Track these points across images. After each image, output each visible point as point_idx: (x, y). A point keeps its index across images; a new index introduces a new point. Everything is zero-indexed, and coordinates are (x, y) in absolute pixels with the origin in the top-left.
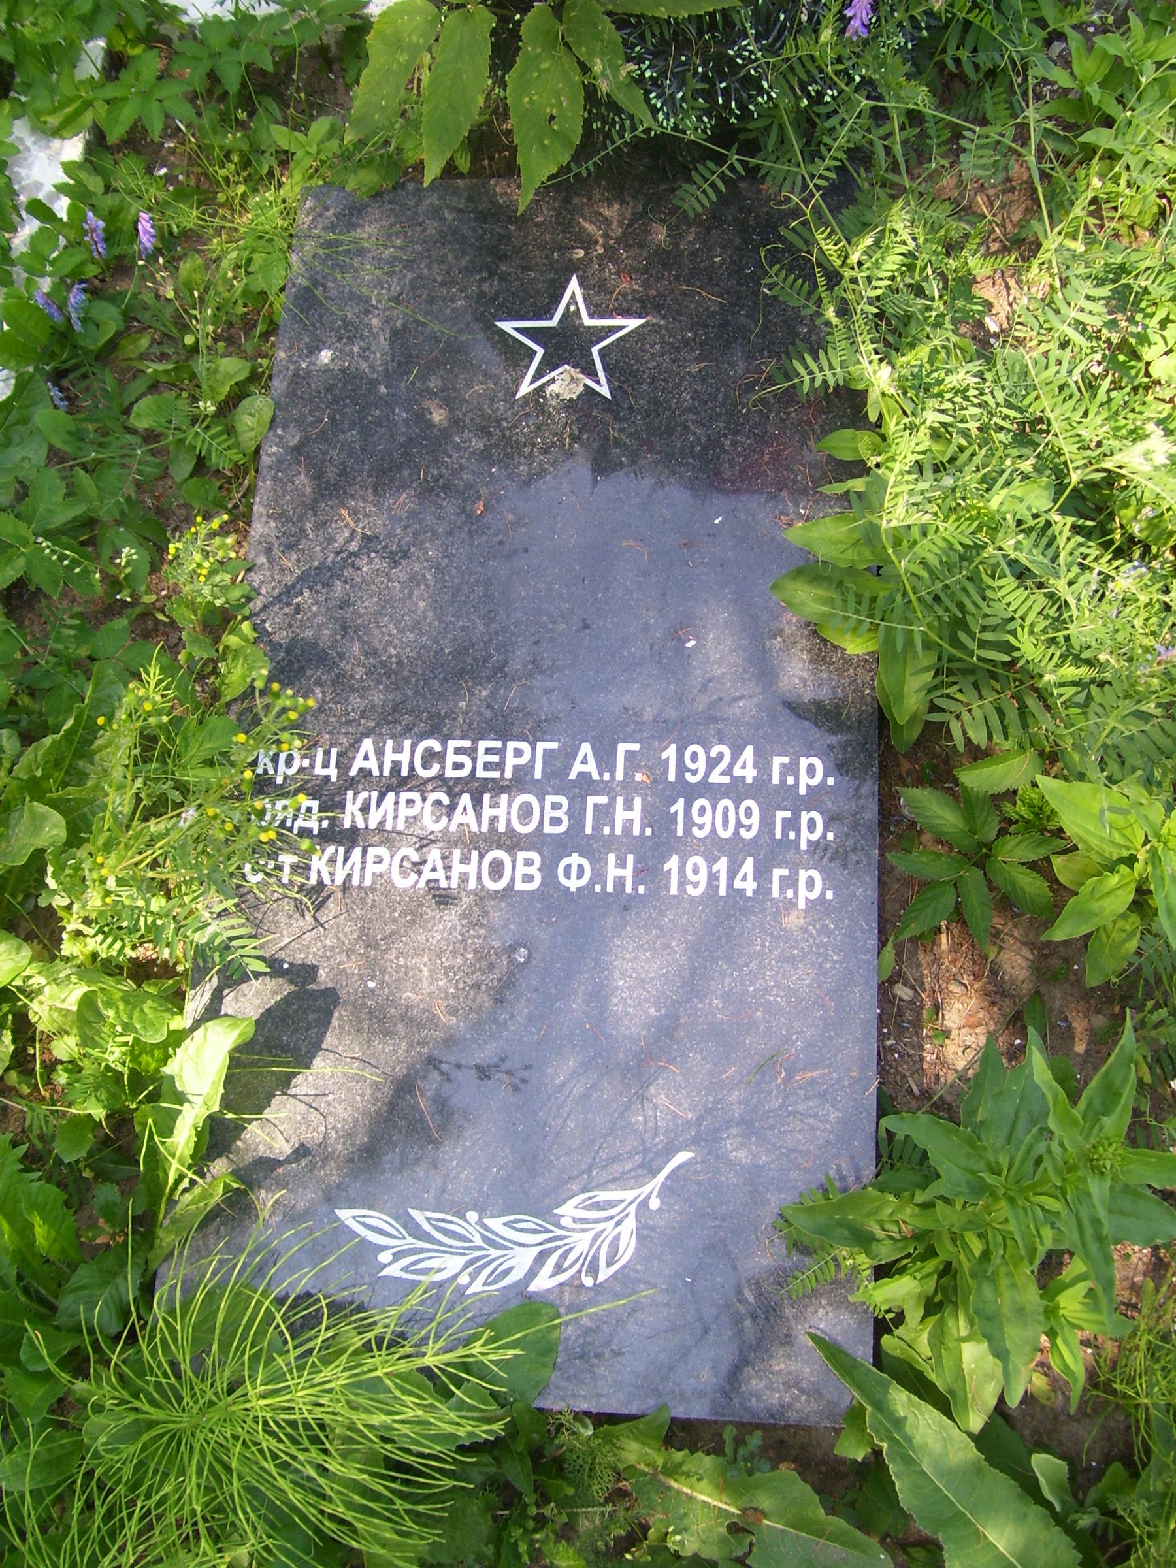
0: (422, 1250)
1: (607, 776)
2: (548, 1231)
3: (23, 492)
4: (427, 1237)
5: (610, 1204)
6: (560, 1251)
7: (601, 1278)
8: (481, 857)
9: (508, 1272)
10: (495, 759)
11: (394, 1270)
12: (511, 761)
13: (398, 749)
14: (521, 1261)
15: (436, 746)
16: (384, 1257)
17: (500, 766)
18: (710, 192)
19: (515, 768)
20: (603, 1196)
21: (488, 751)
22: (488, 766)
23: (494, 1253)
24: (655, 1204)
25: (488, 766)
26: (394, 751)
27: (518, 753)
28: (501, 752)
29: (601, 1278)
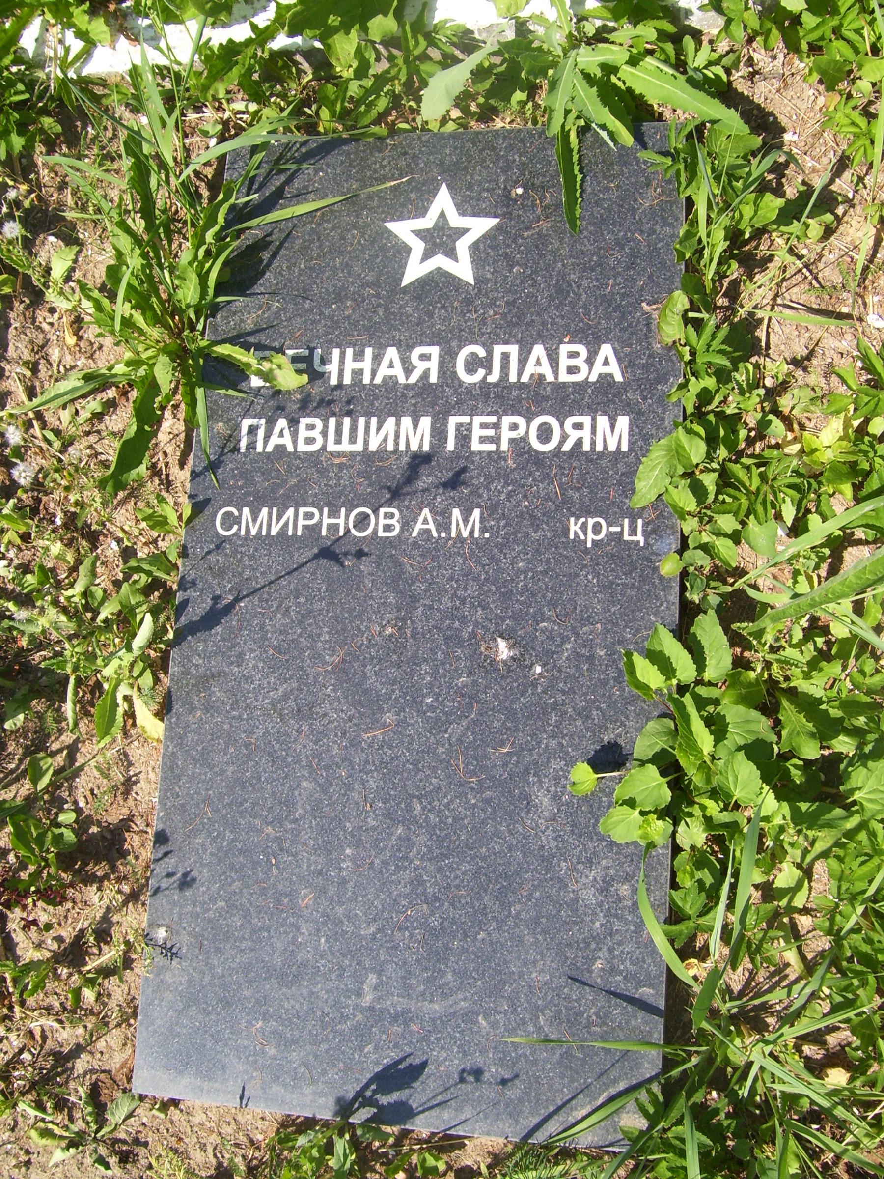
3: (821, 788)
8: (375, 531)
10: (491, 432)
12: (506, 435)
13: (358, 374)
15: (481, 352)
17: (496, 440)
19: (511, 441)
21: (484, 426)
22: (483, 440)
25: (483, 440)
26: (355, 360)
27: (514, 427)
28: (497, 426)
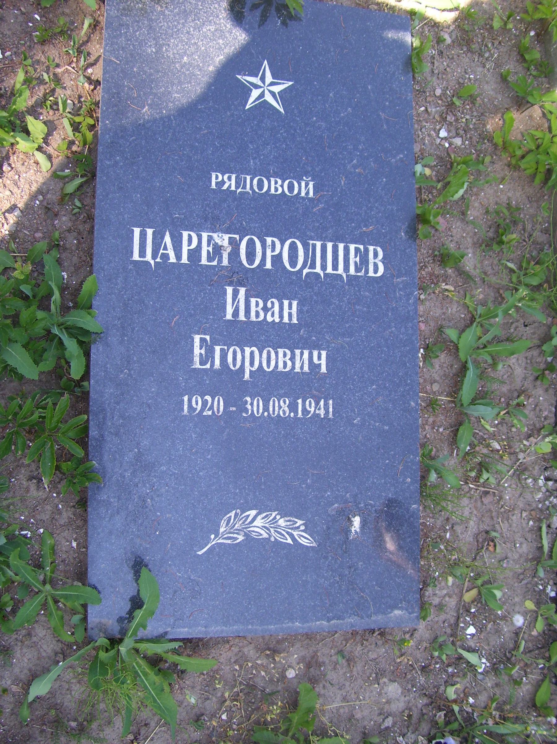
0: (290, 529)
1: (292, 415)
2: (249, 531)
4: (288, 533)
5: (225, 538)
6: (246, 523)
7: (234, 512)
9: (263, 518)
11: (300, 522)
14: (259, 522)
16: (303, 528)
18: (298, 358)
20: (229, 542)
23: (267, 525)
24: (213, 536)
29: (234, 512)
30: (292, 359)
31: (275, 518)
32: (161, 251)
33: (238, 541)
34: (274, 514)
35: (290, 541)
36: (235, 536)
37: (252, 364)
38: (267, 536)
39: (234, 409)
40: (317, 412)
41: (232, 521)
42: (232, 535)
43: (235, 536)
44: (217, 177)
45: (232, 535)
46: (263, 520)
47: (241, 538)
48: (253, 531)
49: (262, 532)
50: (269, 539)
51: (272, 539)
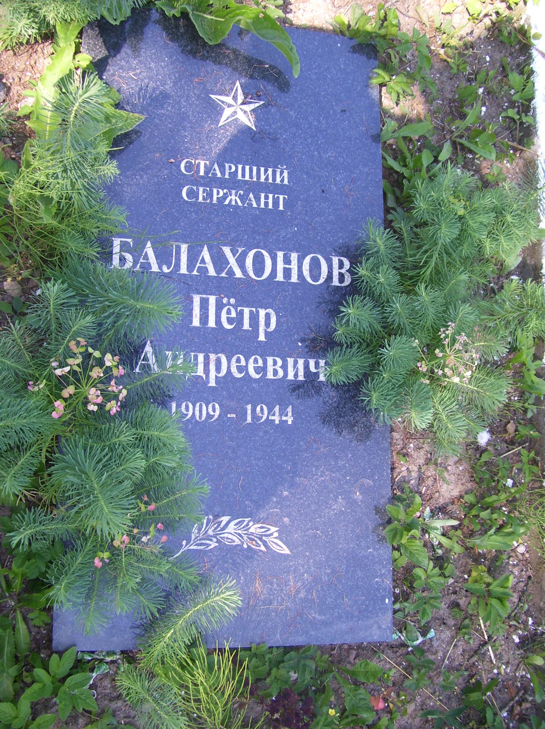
14: (232, 527)
16: (276, 535)
24: (184, 543)
30: (284, 367)
31: (248, 525)
32: (198, 265)
33: (209, 548)
34: (247, 520)
35: (263, 548)
36: (208, 542)
37: (218, 369)
38: (240, 543)
39: (234, 416)
40: (271, 418)
41: (204, 526)
42: (204, 542)
43: (208, 542)
44: (218, 193)
45: (204, 542)
46: (236, 527)
47: (213, 545)
48: (227, 538)
49: (234, 538)
50: (241, 546)
51: (245, 546)
